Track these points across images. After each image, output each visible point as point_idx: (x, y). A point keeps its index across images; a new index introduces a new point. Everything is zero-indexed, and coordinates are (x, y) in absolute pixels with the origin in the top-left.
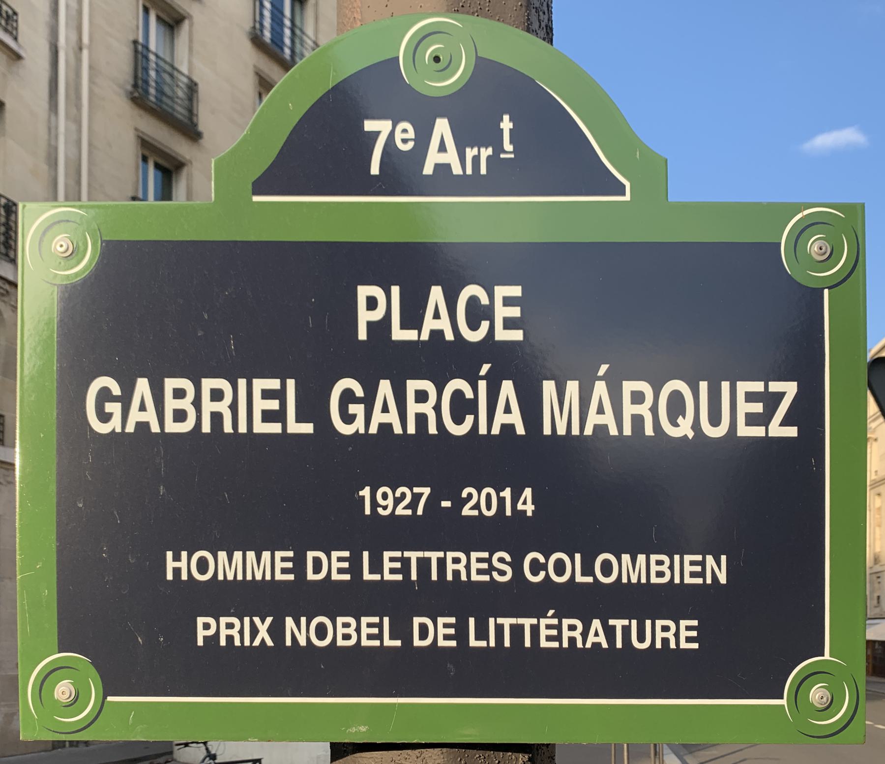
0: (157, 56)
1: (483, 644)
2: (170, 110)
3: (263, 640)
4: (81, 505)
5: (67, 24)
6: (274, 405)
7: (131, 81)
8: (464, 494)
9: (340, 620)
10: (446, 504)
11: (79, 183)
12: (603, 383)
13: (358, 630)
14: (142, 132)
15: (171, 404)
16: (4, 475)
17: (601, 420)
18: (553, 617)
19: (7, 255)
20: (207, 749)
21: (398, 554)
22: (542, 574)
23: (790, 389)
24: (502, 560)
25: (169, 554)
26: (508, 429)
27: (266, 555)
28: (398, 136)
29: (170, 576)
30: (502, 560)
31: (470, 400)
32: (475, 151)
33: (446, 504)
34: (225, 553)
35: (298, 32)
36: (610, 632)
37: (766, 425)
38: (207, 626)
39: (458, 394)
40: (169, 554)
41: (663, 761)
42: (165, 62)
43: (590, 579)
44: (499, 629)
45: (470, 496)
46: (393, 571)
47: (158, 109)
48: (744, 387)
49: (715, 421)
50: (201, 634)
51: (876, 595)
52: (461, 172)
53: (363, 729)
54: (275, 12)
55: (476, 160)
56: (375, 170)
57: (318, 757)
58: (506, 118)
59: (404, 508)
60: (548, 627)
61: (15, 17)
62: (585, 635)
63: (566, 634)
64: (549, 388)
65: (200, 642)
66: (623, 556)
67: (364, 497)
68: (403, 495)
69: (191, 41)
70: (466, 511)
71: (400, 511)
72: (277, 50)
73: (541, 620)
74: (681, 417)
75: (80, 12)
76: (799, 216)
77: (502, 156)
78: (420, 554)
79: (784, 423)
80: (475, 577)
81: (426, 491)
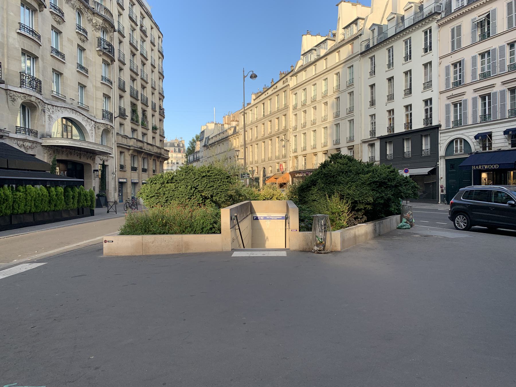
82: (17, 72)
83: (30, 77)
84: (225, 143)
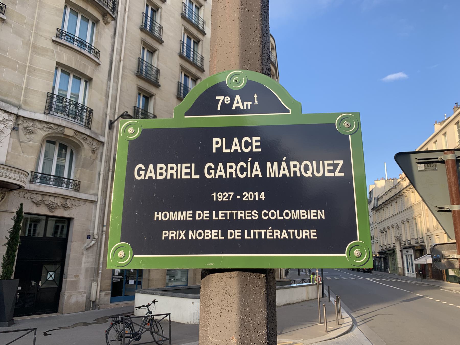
0: (146, 62)
1: (249, 238)
2: (150, 78)
3: (182, 238)
4: (131, 200)
5: (116, 54)
6: (188, 171)
7: (137, 70)
8: (244, 194)
9: (206, 231)
10: (238, 197)
11: (116, 102)
12: (285, 162)
13: (211, 234)
14: (139, 86)
15: (159, 171)
16: (78, 203)
17: (284, 172)
18: (271, 229)
19: (88, 127)
20: (148, 309)
21: (224, 212)
22: (267, 217)
23: (341, 162)
24: (255, 213)
25: (156, 213)
26: (257, 176)
27: (184, 213)
28: (225, 100)
29: (155, 219)
30: (255, 213)
31: (245, 168)
32: (247, 103)
33: (238, 197)
34: (172, 212)
35: (195, 52)
36: (289, 234)
37: (334, 172)
38: (166, 234)
39: (242, 166)
40: (156, 213)
41: (341, 315)
42: (149, 63)
43: (282, 218)
44: (254, 233)
45: (245, 195)
46: (222, 217)
47: (146, 78)
48: (326, 162)
49: (318, 171)
50: (164, 236)
51: (430, 245)
52: (243, 108)
53: (212, 264)
54: (188, 47)
55: (247, 105)
56: (219, 108)
57: (194, 313)
58: (256, 94)
59: (226, 198)
60: (269, 232)
61: (99, 53)
62: (281, 235)
63: (275, 234)
64: (269, 164)
65: (163, 238)
66: (292, 211)
67: (214, 196)
68: (226, 195)
69: (158, 57)
70: (244, 199)
71: (224, 199)
72: (188, 58)
73: (267, 230)
74: (308, 171)
75: (121, 50)
76: (342, 115)
77: (254, 104)
78: (230, 212)
79: (339, 172)
80: (247, 218)
81: (232, 194)
82: (45, 93)
83: (71, 103)
84: (399, 201)
